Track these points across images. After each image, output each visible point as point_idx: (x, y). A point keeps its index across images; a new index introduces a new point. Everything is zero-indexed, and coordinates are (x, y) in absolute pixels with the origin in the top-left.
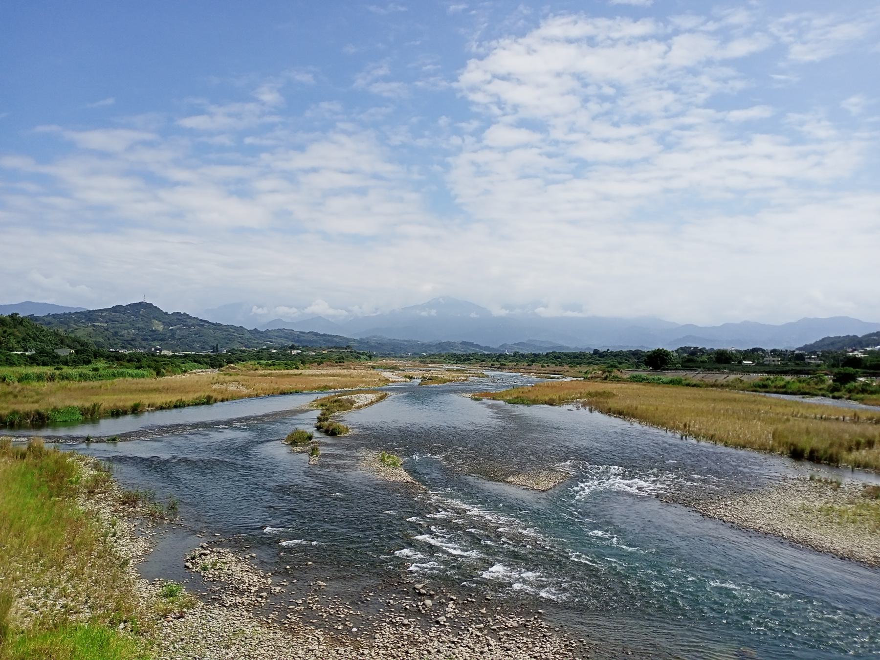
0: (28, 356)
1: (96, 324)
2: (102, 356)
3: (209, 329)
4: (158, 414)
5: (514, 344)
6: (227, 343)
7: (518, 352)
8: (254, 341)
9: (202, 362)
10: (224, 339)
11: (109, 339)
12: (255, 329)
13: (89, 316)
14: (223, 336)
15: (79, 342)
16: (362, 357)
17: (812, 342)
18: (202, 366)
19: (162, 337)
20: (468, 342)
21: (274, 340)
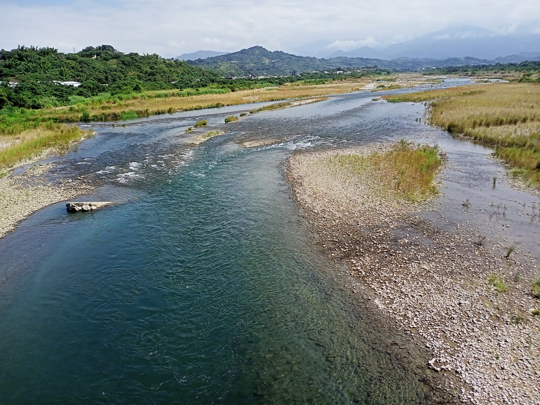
0: (173, 84)
1: (232, 62)
2: (216, 82)
3: (295, 60)
4: (185, 112)
5: (508, 56)
6: (305, 69)
7: (499, 63)
8: (321, 66)
9: (274, 82)
10: (304, 66)
11: (238, 71)
12: (323, 58)
13: (229, 57)
14: (302, 65)
15: (212, 74)
16: (383, 73)
17: (9, 50)
18: (272, 84)
19: (267, 67)
20: (470, 57)
21: (334, 65)
